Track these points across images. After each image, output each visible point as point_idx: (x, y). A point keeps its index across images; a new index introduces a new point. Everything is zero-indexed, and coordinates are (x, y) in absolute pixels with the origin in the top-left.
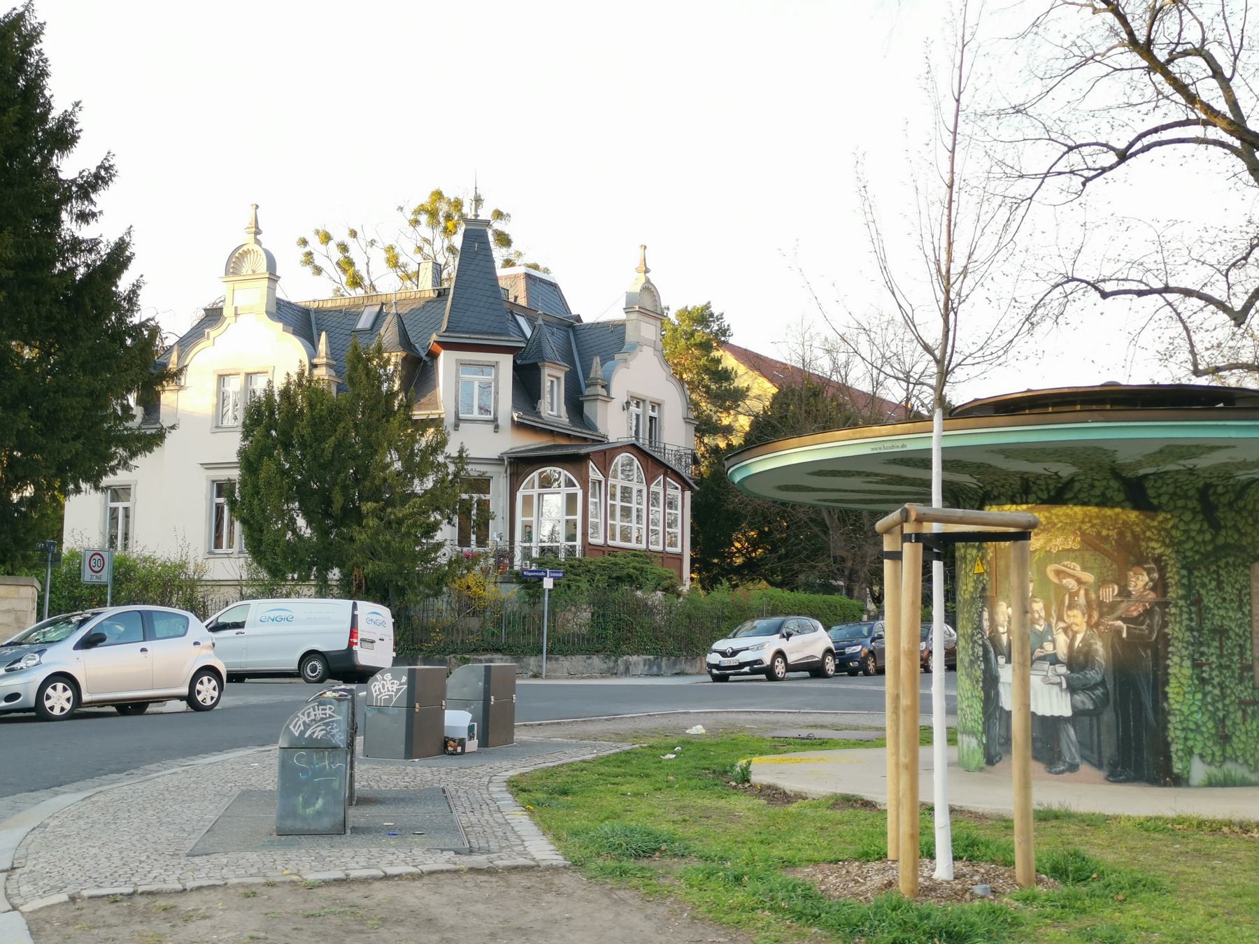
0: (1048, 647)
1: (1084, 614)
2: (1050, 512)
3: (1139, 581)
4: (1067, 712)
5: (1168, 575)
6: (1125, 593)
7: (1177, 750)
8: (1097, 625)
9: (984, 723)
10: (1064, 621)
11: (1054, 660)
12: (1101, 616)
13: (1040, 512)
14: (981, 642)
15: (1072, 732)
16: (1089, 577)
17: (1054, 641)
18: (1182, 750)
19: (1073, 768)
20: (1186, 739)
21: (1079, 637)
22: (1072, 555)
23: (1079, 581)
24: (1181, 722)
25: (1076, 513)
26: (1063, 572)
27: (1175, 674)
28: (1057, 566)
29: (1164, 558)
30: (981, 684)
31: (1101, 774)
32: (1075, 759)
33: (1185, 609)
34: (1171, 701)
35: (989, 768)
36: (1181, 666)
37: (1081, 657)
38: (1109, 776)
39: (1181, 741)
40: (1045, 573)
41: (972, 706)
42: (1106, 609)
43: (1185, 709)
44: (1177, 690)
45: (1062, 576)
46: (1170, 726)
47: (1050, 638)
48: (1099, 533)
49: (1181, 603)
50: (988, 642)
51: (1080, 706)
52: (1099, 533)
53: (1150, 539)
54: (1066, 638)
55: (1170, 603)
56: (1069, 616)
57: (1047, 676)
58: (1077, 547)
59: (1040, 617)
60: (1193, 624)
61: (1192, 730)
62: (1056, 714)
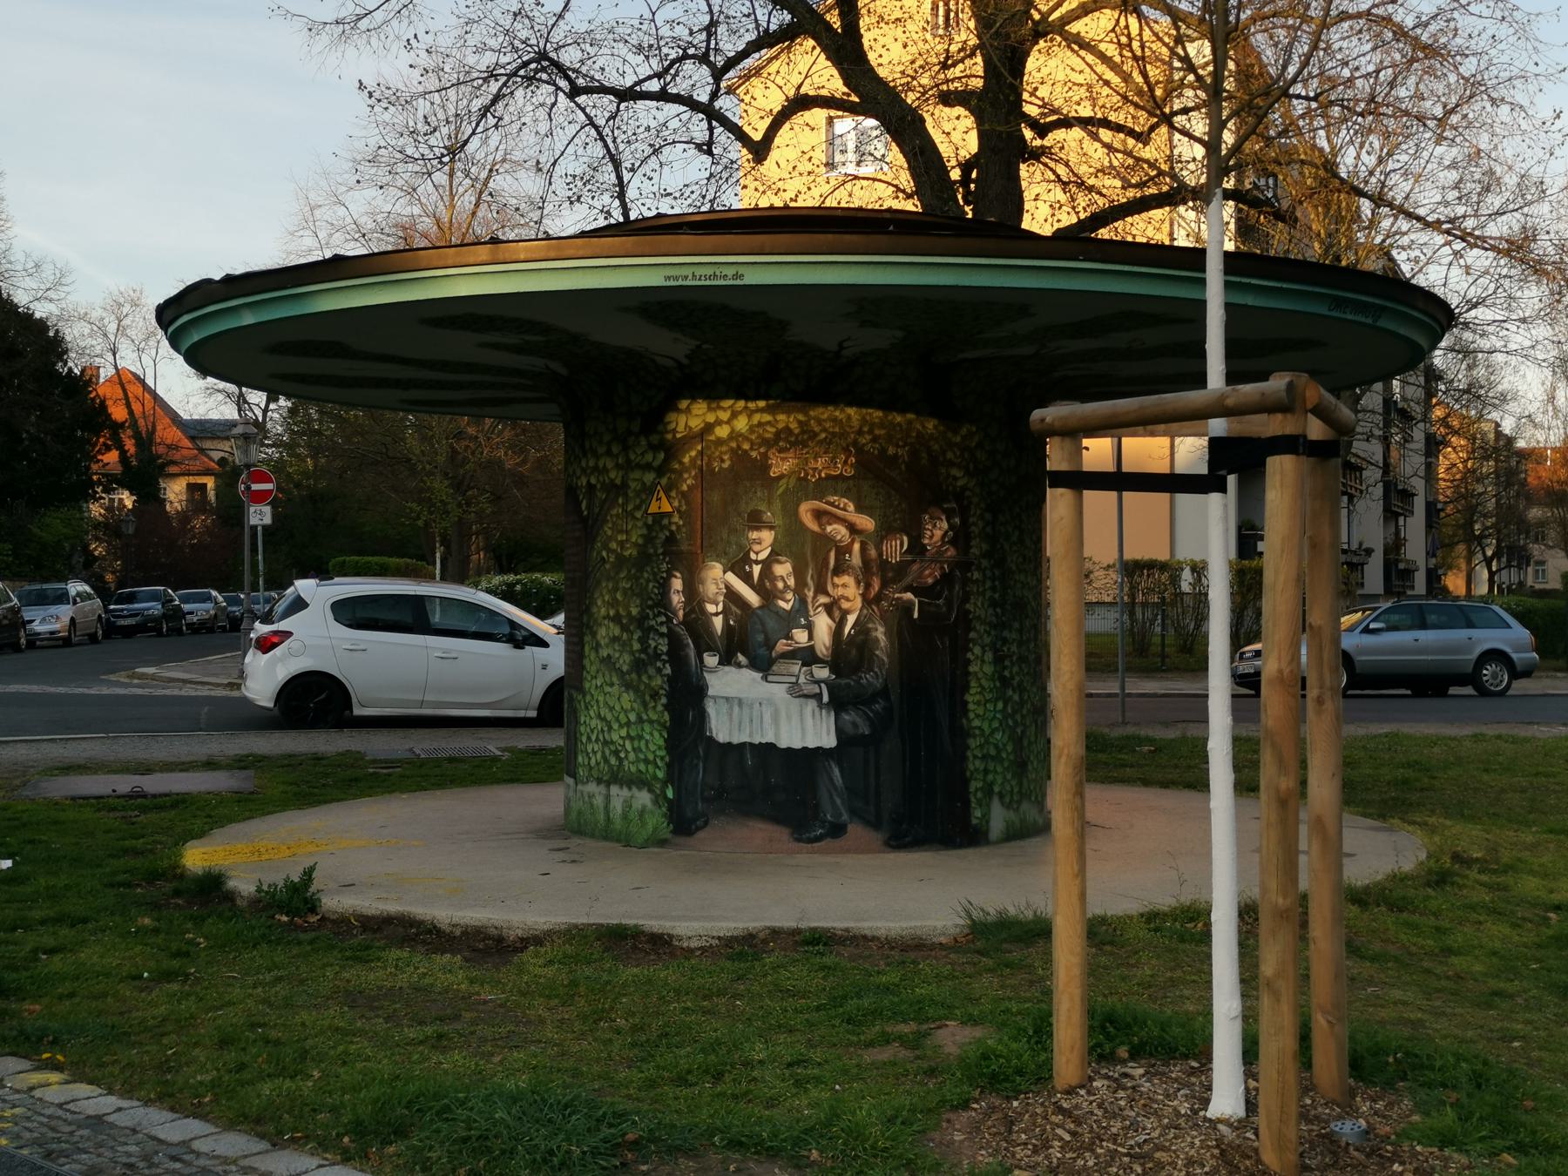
0: (801, 636)
1: (858, 583)
2: (806, 414)
3: (936, 531)
4: (829, 741)
5: (971, 520)
6: (917, 548)
7: (977, 790)
8: (879, 598)
9: (669, 766)
10: (828, 594)
11: (808, 656)
12: (884, 585)
13: (788, 413)
14: (664, 629)
15: (836, 772)
16: (867, 523)
17: (810, 627)
18: (981, 789)
19: (837, 830)
20: (986, 772)
21: (851, 619)
22: (841, 486)
23: (853, 529)
24: (981, 746)
25: (849, 417)
26: (826, 513)
27: (976, 673)
28: (817, 504)
29: (968, 493)
30: (664, 700)
31: (876, 837)
32: (841, 815)
33: (988, 573)
34: (972, 715)
35: (681, 840)
36: (983, 661)
37: (854, 652)
38: (889, 839)
39: (980, 776)
40: (796, 513)
41: (640, 737)
42: (892, 574)
43: (985, 726)
44: (978, 697)
45: (825, 519)
46: (969, 754)
47: (803, 621)
48: (883, 451)
49: (985, 563)
50: (682, 631)
51: (849, 729)
52: (883, 451)
53: (951, 464)
54: (830, 621)
55: (972, 563)
56: (835, 586)
57: (796, 683)
58: (849, 472)
59: (786, 586)
60: (997, 596)
61: (993, 758)
62: (811, 745)
